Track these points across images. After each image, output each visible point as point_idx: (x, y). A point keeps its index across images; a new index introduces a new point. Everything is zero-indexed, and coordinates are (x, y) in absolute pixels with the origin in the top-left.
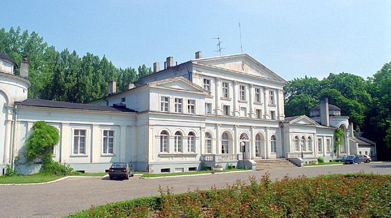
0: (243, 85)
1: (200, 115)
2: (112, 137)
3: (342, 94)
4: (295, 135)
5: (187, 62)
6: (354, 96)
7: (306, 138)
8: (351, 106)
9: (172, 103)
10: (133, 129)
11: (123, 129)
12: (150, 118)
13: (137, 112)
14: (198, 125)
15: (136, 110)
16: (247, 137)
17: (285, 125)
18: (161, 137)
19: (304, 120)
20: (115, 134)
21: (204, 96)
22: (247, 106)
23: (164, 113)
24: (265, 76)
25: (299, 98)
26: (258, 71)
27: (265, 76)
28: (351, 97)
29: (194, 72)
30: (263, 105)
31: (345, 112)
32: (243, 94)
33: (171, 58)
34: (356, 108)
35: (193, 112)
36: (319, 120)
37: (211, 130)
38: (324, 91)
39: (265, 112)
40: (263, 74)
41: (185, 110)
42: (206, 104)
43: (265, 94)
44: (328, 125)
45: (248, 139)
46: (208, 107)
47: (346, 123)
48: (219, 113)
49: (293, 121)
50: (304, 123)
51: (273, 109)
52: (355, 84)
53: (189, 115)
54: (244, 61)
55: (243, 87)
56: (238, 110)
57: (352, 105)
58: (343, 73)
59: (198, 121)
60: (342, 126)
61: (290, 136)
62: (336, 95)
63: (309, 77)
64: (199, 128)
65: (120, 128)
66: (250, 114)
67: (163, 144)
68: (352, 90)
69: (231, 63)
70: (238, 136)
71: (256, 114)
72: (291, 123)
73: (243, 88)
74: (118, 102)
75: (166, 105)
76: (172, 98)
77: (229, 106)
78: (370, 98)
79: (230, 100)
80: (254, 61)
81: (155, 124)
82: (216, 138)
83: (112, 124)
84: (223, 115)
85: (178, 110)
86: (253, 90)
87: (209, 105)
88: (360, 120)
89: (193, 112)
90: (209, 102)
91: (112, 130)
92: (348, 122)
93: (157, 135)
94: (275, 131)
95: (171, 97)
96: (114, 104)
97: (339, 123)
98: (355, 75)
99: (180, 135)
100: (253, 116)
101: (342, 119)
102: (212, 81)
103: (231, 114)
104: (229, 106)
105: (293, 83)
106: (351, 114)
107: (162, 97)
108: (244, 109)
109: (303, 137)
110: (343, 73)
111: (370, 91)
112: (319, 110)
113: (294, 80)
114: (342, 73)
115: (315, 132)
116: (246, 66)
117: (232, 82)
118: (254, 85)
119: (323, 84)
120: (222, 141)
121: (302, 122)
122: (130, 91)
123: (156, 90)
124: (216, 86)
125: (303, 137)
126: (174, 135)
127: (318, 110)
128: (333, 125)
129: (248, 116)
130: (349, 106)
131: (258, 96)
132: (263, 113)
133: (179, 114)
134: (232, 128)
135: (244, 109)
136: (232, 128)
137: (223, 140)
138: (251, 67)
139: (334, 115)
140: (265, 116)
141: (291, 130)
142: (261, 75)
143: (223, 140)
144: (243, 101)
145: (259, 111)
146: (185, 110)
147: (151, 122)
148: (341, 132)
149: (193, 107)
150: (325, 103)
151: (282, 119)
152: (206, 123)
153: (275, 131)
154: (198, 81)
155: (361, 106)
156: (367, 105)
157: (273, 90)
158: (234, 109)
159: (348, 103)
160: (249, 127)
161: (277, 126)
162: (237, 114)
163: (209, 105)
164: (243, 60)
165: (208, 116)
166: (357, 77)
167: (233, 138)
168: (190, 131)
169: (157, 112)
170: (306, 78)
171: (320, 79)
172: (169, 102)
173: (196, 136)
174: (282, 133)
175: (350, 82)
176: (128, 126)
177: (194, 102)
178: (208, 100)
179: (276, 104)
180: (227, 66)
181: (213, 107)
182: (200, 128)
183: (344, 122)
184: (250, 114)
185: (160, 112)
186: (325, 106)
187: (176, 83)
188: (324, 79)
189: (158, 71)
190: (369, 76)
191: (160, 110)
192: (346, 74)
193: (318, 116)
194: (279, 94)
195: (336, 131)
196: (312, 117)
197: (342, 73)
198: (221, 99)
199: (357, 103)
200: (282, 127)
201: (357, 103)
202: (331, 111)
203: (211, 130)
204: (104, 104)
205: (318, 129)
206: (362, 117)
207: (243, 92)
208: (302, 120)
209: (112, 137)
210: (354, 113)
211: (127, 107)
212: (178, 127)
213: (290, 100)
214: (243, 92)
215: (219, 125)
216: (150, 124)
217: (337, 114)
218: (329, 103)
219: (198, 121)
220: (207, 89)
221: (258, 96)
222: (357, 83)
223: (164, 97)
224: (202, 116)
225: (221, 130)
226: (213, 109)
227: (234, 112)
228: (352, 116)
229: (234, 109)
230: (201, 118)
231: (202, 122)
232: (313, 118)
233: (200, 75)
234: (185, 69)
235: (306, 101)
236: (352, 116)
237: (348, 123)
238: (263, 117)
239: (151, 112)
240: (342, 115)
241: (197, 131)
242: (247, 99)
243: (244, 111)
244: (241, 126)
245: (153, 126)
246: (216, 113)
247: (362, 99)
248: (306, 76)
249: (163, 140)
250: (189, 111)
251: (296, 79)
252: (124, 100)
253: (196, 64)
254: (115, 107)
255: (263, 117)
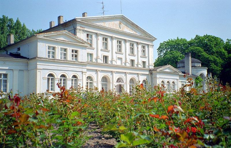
0: (120, 40)
1: (82, 62)
2: (6, 79)
3: (205, 50)
4: (162, 80)
5: (72, 20)
6: (214, 52)
7: (166, 82)
8: (211, 61)
9: (69, 53)
10: (25, 73)
11: (16, 73)
12: (38, 63)
13: (28, 59)
14: (80, 70)
15: (28, 57)
16: (123, 80)
17: (154, 72)
18: (48, 79)
19: (169, 68)
20: (9, 76)
21: (85, 48)
22: (123, 57)
23: (51, 59)
24: (138, 34)
25: (171, 54)
26: (132, 30)
27: (138, 34)
28: (213, 53)
29: (78, 27)
30: (136, 56)
31: (205, 63)
32: (144, 52)
33: (61, 17)
34: (215, 62)
35: (76, 59)
36: (183, 70)
37: (93, 74)
38: (191, 48)
39: (138, 62)
40: (136, 32)
41: (69, 58)
42: (104, 56)
43: (138, 48)
44: (190, 73)
45: (123, 82)
46: (90, 56)
47: (205, 72)
48: (128, 65)
49: (161, 69)
50: (169, 71)
51: (144, 60)
52: (215, 43)
53: (72, 61)
54: (121, 21)
55: (144, 47)
56: (128, 62)
57: (212, 59)
58: (207, 35)
59: (80, 67)
60: (202, 75)
61: (157, 80)
62: (200, 52)
63: (180, 38)
64: (81, 73)
65: (13, 72)
66: (125, 63)
67: (50, 85)
68: (212, 48)
69: (110, 22)
70: (115, 80)
71: (130, 63)
72: (158, 70)
73: (120, 42)
74: (14, 51)
75: (53, 53)
76: (69, 50)
77: (134, 60)
78: (226, 54)
79: (146, 58)
80: (129, 21)
81: (42, 68)
82: (96, 81)
83: (7, 68)
84: (103, 62)
85: (51, 56)
86: (128, 44)
87: (91, 55)
88: (217, 71)
89: (76, 59)
90: (91, 53)
91: (7, 73)
92: (207, 72)
93: (44, 77)
94: (146, 77)
95: (56, 46)
96: (10, 53)
97: (199, 72)
98: (216, 36)
99: (53, 77)
100: (128, 65)
101: (202, 69)
102: (109, 39)
103: (109, 62)
104: (134, 60)
105: (168, 42)
106: (211, 67)
107: (61, 48)
108: (120, 59)
109: (168, 82)
110: (207, 35)
111: (228, 49)
112: (184, 63)
113: (168, 41)
114: (206, 35)
115: (178, 78)
116: (123, 25)
117: (111, 38)
118: (129, 40)
119: (191, 43)
120: (130, 85)
121: (167, 70)
122: (24, 42)
123: (43, 40)
124: (97, 40)
125: (168, 82)
126: (71, 78)
127: (183, 62)
128: (194, 74)
129: (123, 64)
130: (210, 60)
131: (132, 49)
132: (136, 62)
133: (64, 61)
134: (124, 75)
135: (120, 59)
136: (124, 75)
137: (103, 83)
138: (126, 26)
139: (195, 66)
140: (137, 65)
141: (158, 76)
142: (98, 24)
143: (103, 83)
144: (120, 52)
145: (132, 61)
146: (69, 58)
147: (39, 67)
148: (201, 79)
149: (76, 56)
150: (188, 57)
151: (152, 67)
152: (87, 69)
153: (146, 77)
154: (81, 35)
155: (219, 60)
156: (224, 60)
157: (133, 43)
158: (112, 58)
159: (208, 58)
160: (111, 72)
161: (147, 73)
162: (114, 63)
163: (91, 55)
164: (120, 20)
165: (90, 63)
166: (217, 38)
167: (111, 81)
168: (162, 80)
169: (44, 58)
170: (178, 39)
171: (189, 40)
172: (55, 51)
173: (79, 78)
174: (152, 78)
175: (211, 42)
176: (20, 70)
177: (76, 52)
178: (90, 51)
179: (147, 55)
180: (107, 25)
181: (95, 56)
182: (82, 72)
183: (204, 71)
184: (125, 63)
185: (47, 59)
186: (188, 59)
187: (62, 36)
188: (192, 39)
189: (53, 27)
190: (228, 39)
191: (71, 60)
192: (209, 36)
193: (183, 67)
194: (150, 48)
195: (197, 78)
196: (179, 68)
197: (206, 35)
198: (101, 50)
199: (216, 58)
200: (151, 74)
201: (216, 58)
202: (193, 63)
203: (93, 74)
204: (5, 53)
205: (180, 76)
206: (219, 68)
207: (144, 50)
208: (168, 68)
209: (6, 79)
210: (213, 66)
211: (22, 55)
212: (74, 72)
213: (164, 55)
214: (144, 50)
215: (99, 70)
216: (157, 77)
217: (199, 65)
218: (192, 57)
219: (80, 67)
220: (89, 42)
221: (132, 49)
222: (217, 42)
223: (63, 48)
224: (84, 63)
225: (101, 75)
226: (94, 58)
227: (112, 61)
228: (211, 68)
229: (112, 58)
230: (82, 64)
231: (83, 67)
232: (179, 69)
233: (83, 30)
234: (69, 25)
235: (174, 55)
236: (211, 68)
237: (207, 73)
238: (136, 66)
239: (39, 58)
240: (202, 66)
241: (79, 75)
242: (135, 53)
243: (120, 61)
244: (130, 73)
245: (159, 78)
246: (97, 61)
247: (220, 54)
248: (178, 37)
249: (50, 81)
250: (73, 59)
251: (170, 40)
252: (19, 49)
253: (79, 22)
254: (12, 55)
255: (136, 66)
